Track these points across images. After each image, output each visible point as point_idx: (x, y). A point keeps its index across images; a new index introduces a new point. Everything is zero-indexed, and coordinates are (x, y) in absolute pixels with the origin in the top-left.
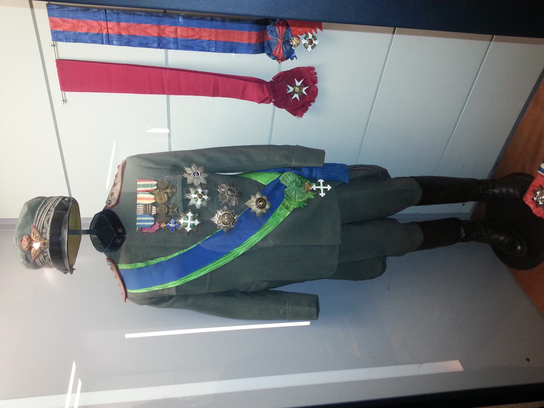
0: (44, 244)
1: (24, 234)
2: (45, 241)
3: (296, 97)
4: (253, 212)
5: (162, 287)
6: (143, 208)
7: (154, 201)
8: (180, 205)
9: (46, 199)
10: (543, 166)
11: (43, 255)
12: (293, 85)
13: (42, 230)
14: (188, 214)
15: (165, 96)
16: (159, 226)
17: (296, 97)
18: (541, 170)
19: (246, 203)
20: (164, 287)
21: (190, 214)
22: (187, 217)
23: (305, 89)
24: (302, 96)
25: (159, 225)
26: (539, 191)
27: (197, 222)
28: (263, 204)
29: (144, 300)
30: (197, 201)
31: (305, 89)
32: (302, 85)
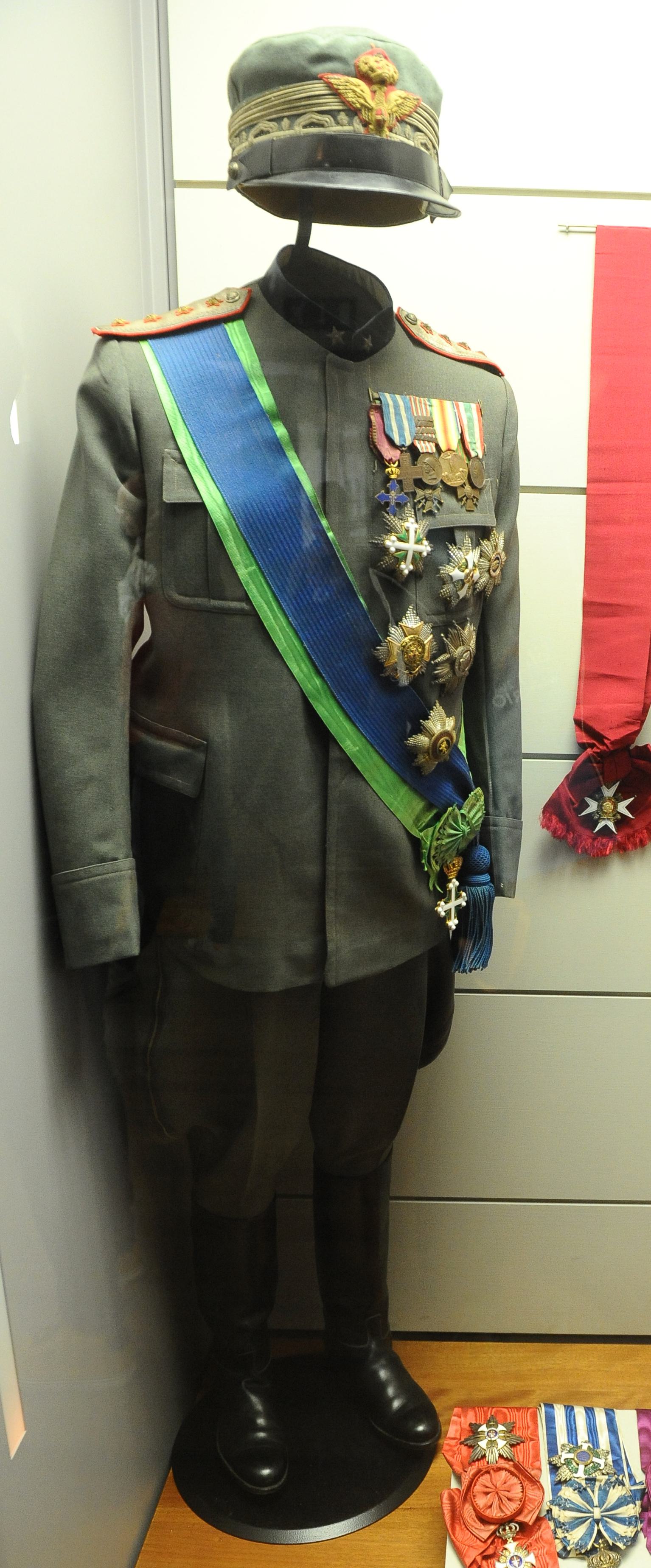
0: (380, 125)
1: (399, 68)
2: (388, 127)
3: (589, 806)
4: (420, 724)
5: (192, 459)
6: (425, 415)
7: (443, 447)
8: (443, 520)
9: (241, 94)
10: (559, 1409)
11: (339, 111)
12: (617, 798)
13: (411, 125)
14: (425, 542)
15: (583, 484)
16: (391, 460)
17: (589, 806)
18: (550, 1410)
19: (438, 704)
20: (196, 467)
21: (425, 548)
22: (418, 541)
23: (611, 825)
24: (591, 821)
25: (394, 459)
26: (506, 1427)
27: (406, 568)
28: (441, 751)
29: (131, 396)
30: (459, 568)
31: (611, 825)
32: (619, 817)
